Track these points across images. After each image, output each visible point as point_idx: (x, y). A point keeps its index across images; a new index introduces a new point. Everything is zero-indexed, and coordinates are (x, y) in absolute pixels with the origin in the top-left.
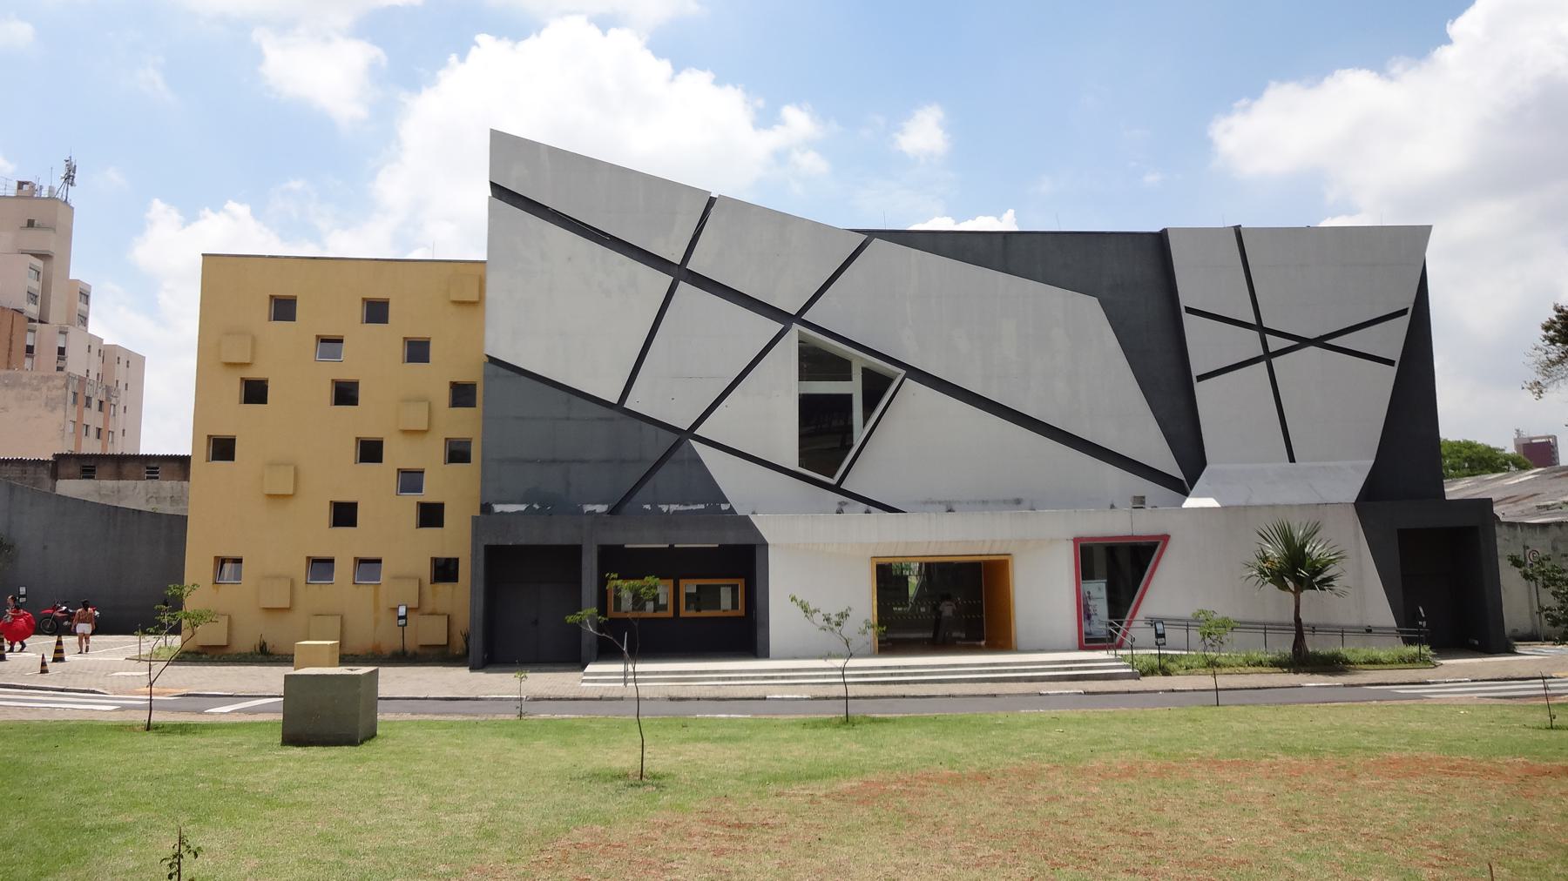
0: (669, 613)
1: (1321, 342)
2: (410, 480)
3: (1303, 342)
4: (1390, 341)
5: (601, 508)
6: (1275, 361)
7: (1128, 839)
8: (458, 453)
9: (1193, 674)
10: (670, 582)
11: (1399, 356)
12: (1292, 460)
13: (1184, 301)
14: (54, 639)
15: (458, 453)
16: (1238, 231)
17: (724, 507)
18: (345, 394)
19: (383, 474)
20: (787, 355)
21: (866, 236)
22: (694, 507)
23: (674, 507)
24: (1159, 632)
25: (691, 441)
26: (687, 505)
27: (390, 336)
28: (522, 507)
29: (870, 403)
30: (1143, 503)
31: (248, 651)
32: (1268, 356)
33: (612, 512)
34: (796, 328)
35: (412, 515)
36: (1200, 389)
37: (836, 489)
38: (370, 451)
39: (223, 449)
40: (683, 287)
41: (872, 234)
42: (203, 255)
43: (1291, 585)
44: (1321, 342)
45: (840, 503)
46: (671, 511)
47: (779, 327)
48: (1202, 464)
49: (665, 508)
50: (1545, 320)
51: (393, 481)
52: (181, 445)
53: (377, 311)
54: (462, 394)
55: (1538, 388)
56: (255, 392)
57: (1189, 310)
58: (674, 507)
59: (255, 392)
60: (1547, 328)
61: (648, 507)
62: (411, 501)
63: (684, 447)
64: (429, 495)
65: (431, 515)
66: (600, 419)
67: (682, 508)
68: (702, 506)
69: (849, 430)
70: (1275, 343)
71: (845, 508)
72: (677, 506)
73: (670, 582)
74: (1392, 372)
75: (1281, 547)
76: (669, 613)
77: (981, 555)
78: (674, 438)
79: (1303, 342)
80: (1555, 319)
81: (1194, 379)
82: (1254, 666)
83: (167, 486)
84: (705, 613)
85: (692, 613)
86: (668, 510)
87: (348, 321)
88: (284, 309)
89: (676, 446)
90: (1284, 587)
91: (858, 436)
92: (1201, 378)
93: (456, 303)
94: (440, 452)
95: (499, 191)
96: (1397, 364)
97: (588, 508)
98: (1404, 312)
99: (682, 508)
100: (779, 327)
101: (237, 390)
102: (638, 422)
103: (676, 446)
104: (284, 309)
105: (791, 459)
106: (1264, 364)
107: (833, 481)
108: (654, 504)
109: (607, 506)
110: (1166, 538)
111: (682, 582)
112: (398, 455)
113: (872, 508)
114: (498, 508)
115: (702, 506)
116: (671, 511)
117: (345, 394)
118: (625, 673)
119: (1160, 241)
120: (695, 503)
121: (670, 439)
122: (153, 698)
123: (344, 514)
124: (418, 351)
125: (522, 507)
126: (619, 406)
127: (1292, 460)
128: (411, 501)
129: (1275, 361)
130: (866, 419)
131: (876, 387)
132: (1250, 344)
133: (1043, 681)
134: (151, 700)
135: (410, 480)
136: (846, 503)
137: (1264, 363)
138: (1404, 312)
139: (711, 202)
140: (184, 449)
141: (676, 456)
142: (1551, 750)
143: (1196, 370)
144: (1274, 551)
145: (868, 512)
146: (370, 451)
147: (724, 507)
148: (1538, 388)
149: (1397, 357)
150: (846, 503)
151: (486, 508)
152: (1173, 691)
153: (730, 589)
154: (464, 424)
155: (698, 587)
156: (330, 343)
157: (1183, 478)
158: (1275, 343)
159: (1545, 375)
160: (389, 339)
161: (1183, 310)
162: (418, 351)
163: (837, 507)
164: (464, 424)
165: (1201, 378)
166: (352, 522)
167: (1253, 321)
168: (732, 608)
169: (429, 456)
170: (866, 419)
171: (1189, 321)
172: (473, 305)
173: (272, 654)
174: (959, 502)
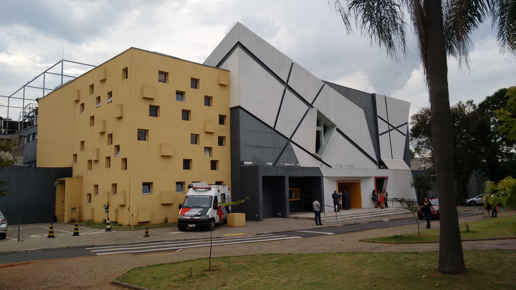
5: (271, 164)
7: (361, 3)
8: (221, 141)
12: (392, 159)
14: (49, 225)
19: (199, 148)
23: (288, 164)
28: (251, 163)
31: (159, 222)
32: (390, 131)
33: (274, 164)
36: (380, 137)
38: (195, 139)
49: (285, 164)
56: (154, 111)
65: (214, 165)
77: (348, 181)
79: (394, 128)
87: (186, 86)
88: (164, 76)
92: (381, 135)
99: (289, 165)
108: (283, 163)
112: (205, 141)
114: (245, 163)
117: (186, 115)
118: (336, 216)
119: (373, 97)
123: (187, 164)
125: (251, 163)
127: (392, 159)
133: (280, 232)
143: (380, 133)
152: (36, 78)
155: (341, 205)
157: (377, 161)
162: (208, 100)
169: (213, 142)
173: (122, 225)
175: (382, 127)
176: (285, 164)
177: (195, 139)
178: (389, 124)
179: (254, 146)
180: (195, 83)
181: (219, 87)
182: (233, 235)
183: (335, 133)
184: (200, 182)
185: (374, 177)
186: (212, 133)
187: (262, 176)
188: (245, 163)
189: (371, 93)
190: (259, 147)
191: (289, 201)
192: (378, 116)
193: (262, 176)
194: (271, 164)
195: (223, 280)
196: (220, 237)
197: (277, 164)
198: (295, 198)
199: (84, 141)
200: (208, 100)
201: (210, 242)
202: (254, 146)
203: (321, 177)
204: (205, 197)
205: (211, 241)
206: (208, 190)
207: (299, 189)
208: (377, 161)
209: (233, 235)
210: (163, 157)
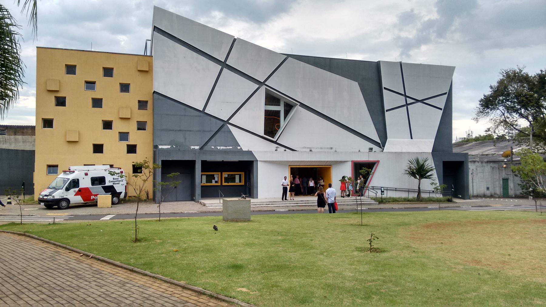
0: (219, 184)
1: (422, 101)
2: (124, 136)
3: (417, 101)
4: (441, 102)
5: (197, 148)
6: (409, 106)
8: (141, 126)
9: (391, 204)
10: (220, 173)
11: (444, 107)
12: (412, 138)
13: (384, 86)
15: (141, 126)
16: (401, 63)
17: (239, 148)
18: (97, 103)
20: (261, 95)
21: (286, 56)
22: (229, 148)
23: (222, 148)
24: (382, 191)
25: (228, 125)
26: (226, 147)
27: (114, 82)
28: (169, 147)
29: (286, 114)
30: (372, 150)
32: (407, 105)
33: (201, 149)
34: (264, 87)
35: (125, 149)
36: (387, 114)
37: (275, 142)
39: (48, 123)
40: (225, 70)
41: (289, 56)
42: (37, 47)
43: (418, 177)
44: (422, 101)
45: (276, 147)
46: (221, 149)
47: (258, 86)
48: (386, 138)
49: (219, 148)
50: (480, 99)
51: (117, 136)
52: (31, 121)
53: (108, 72)
54: (142, 105)
55: (477, 120)
57: (385, 88)
58: (222, 148)
59: (61, 102)
60: (480, 102)
61: (213, 147)
62: (124, 144)
63: (225, 127)
64: (131, 142)
66: (196, 116)
67: (225, 148)
68: (231, 147)
69: (279, 121)
70: (409, 101)
71: (278, 149)
72: (223, 147)
73: (220, 173)
74: (441, 112)
75: (416, 166)
76: (219, 184)
78: (222, 123)
80: (483, 99)
81: (385, 111)
82: (407, 201)
83: (28, 138)
84: (230, 184)
85: (226, 184)
86: (220, 148)
87: (98, 76)
89: (222, 126)
90: (415, 177)
91: (282, 123)
92: (387, 111)
93: (139, 71)
94: (135, 126)
95: (156, 29)
96: (443, 110)
97: (192, 147)
98: (445, 93)
99: (225, 148)
100: (258, 86)
101: (53, 101)
102: (209, 117)
103: (222, 126)
104: (71, 69)
105: (262, 133)
106: (405, 107)
107: (274, 140)
108: (215, 146)
109: (199, 147)
110: (378, 162)
111: (223, 173)
112: (118, 127)
113: (286, 149)
114: (160, 147)
115: (231, 147)
116: (221, 149)
120: (229, 146)
121: (220, 124)
122: (21, 220)
124: (125, 88)
125: (169, 147)
126: (203, 112)
127: (412, 138)
128: (124, 144)
129: (409, 106)
130: (285, 117)
131: (289, 108)
132: (401, 101)
134: (21, 221)
135: (124, 136)
136: (278, 147)
137: (406, 107)
138: (445, 93)
139: (235, 40)
140: (33, 123)
141: (223, 130)
142: (467, 219)
144: (414, 166)
145: (285, 150)
146: (107, 125)
147: (239, 148)
148: (477, 120)
149: (443, 108)
150: (278, 147)
151: (156, 147)
153: (239, 176)
154: (144, 116)
156: (90, 84)
157: (380, 143)
158: (409, 101)
159: (477, 115)
160: (114, 82)
161: (383, 88)
163: (275, 149)
164: (144, 116)
165: (387, 111)
166: (95, 151)
167: (404, 93)
168: (239, 182)
169: (131, 128)
170: (285, 117)
171: (384, 91)
172: (146, 72)
174: (314, 148)
175: (389, 100)
176: (219, 148)
177: (107, 125)
178: (406, 97)
179: (173, 130)
180: (108, 72)
181: (138, 73)
182: (59, 214)
183: (298, 108)
184: (94, 165)
185: (352, 161)
186: (128, 119)
187: (162, 161)
188: (160, 147)
189: (376, 61)
190: (180, 130)
191: (200, 187)
192: (384, 87)
193: (162, 161)
194: (197, 148)
195: (300, 249)
196: (32, 215)
197: (206, 148)
198: (240, 181)
199: (455, 67)
200: (125, 88)
201: (21, 218)
202: (173, 130)
203: (253, 161)
204: (65, 179)
205: (21, 217)
206: (72, 173)
207: (220, 173)
208: (380, 142)
209: (59, 214)
210: (69, 142)
